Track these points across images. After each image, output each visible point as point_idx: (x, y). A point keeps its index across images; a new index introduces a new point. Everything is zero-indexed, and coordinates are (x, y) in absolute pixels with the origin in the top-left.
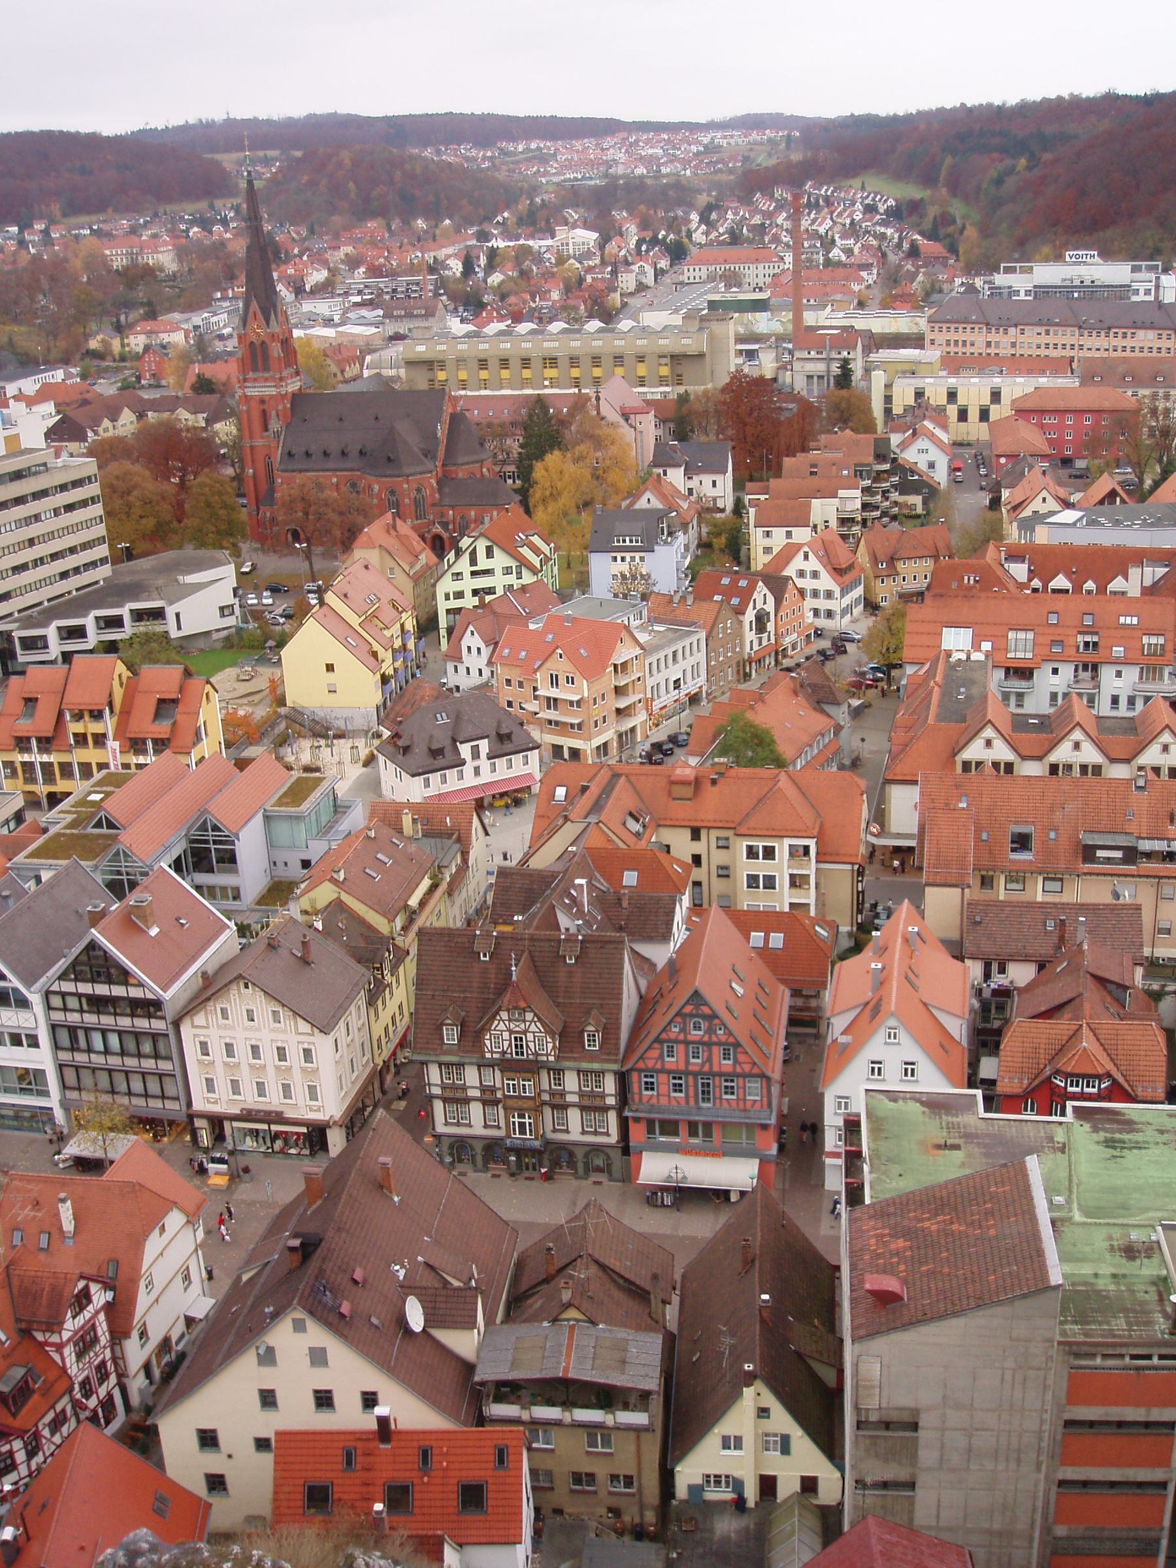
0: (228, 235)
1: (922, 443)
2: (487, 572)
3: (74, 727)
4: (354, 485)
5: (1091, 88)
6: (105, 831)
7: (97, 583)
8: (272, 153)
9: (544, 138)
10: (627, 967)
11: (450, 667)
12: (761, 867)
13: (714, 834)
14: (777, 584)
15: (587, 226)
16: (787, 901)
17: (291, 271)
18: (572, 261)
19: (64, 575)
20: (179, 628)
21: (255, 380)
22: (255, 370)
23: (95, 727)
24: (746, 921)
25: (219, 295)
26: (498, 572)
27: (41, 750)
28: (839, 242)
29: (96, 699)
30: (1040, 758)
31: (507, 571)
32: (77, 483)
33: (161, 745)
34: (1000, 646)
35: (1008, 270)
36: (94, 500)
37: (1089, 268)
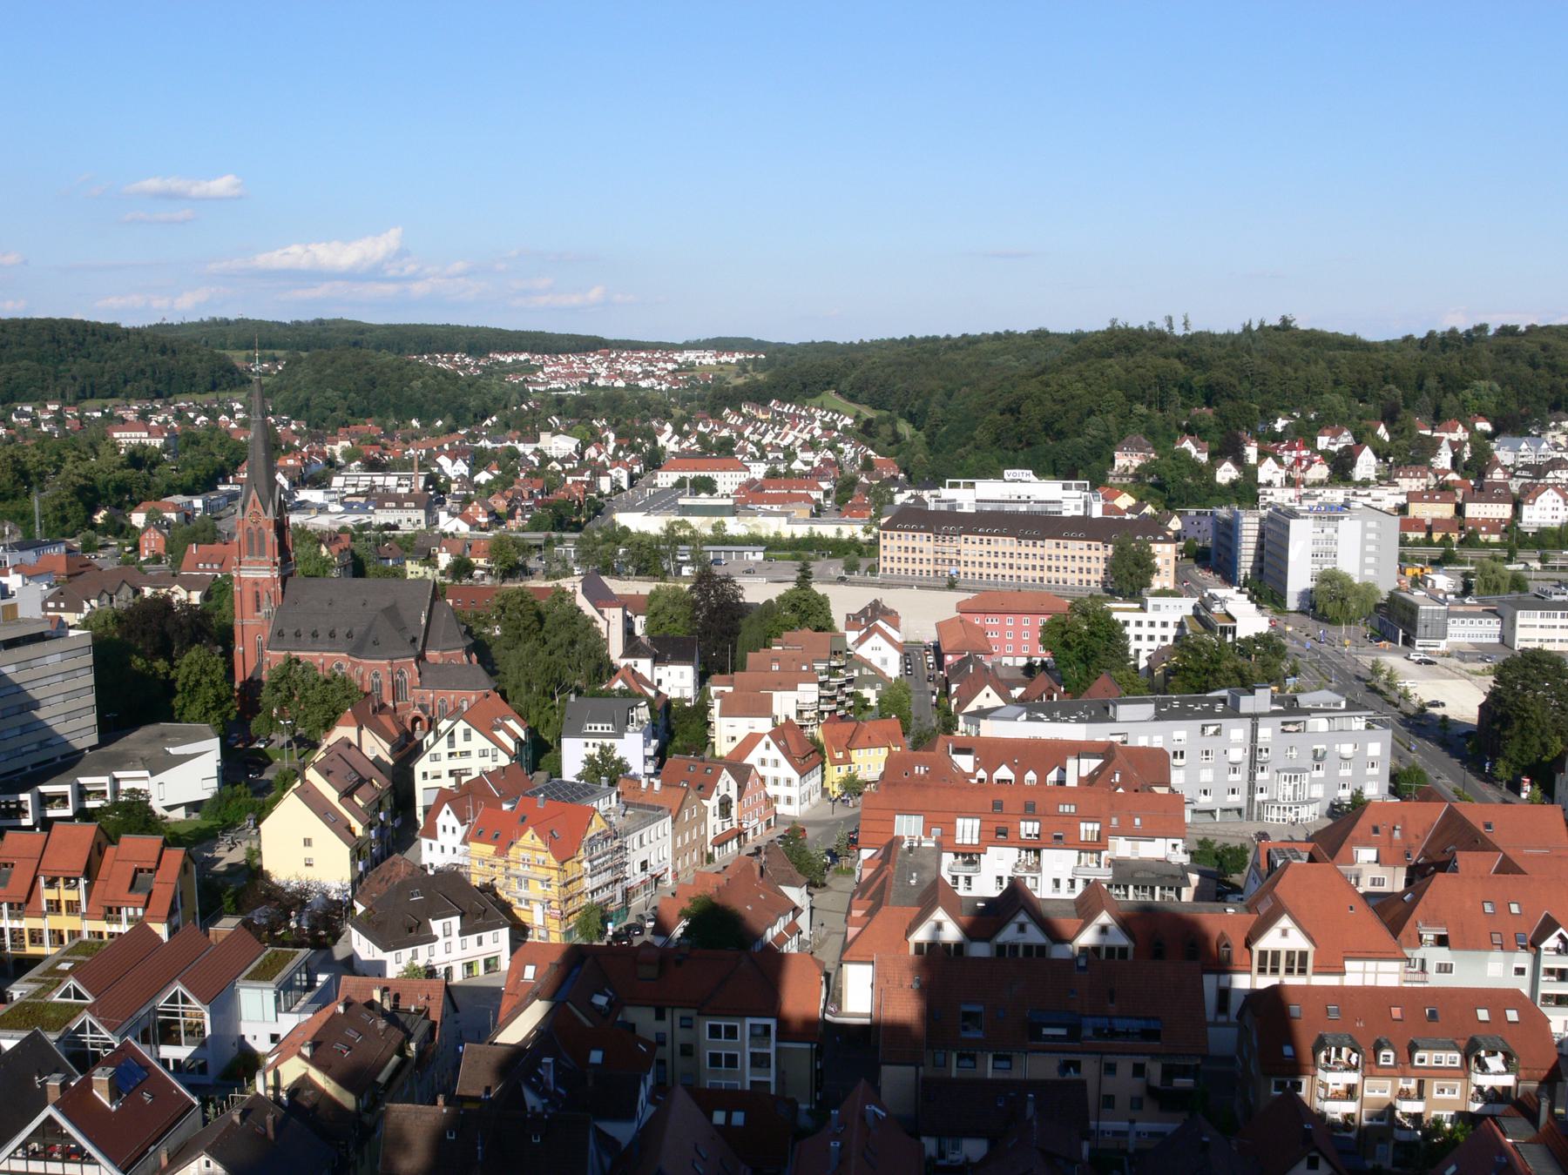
0: (233, 426)
1: (876, 640)
5: (1023, 325)
6: (72, 1000)
8: (279, 353)
9: (532, 351)
10: (592, 1146)
12: (723, 1046)
13: (678, 1013)
14: (742, 773)
15: (568, 431)
16: (748, 1078)
18: (554, 464)
21: (250, 563)
22: (251, 555)
24: (709, 1100)
26: (475, 754)
28: (801, 455)
30: (987, 939)
34: (949, 831)
35: (953, 486)
37: (1023, 488)
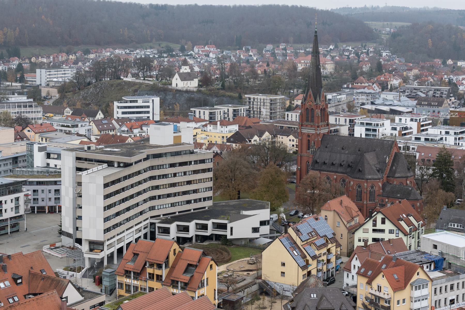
2: (382, 231)
3: (150, 270)
4: (344, 181)
7: (205, 208)
11: (345, 274)
17: (382, 79)
19: (189, 202)
20: (232, 234)
21: (307, 126)
22: (307, 121)
23: (157, 272)
25: (345, 86)
26: (387, 231)
27: (136, 278)
29: (162, 260)
31: (391, 232)
32: (203, 161)
33: (185, 286)
36: (209, 170)
